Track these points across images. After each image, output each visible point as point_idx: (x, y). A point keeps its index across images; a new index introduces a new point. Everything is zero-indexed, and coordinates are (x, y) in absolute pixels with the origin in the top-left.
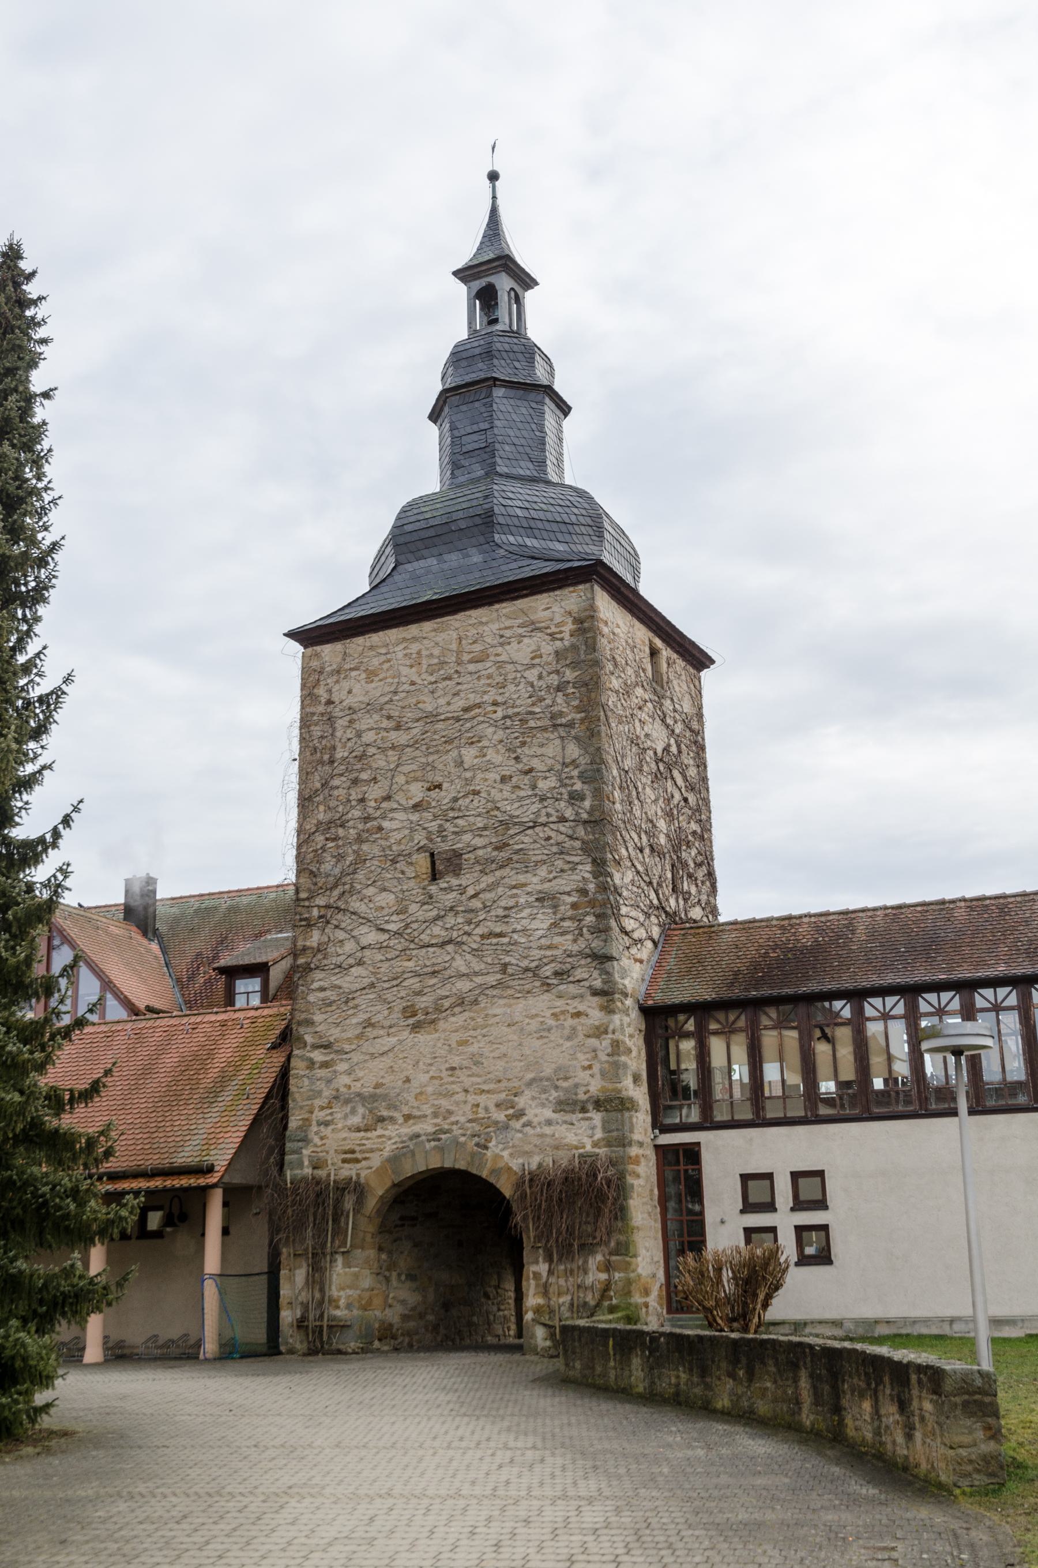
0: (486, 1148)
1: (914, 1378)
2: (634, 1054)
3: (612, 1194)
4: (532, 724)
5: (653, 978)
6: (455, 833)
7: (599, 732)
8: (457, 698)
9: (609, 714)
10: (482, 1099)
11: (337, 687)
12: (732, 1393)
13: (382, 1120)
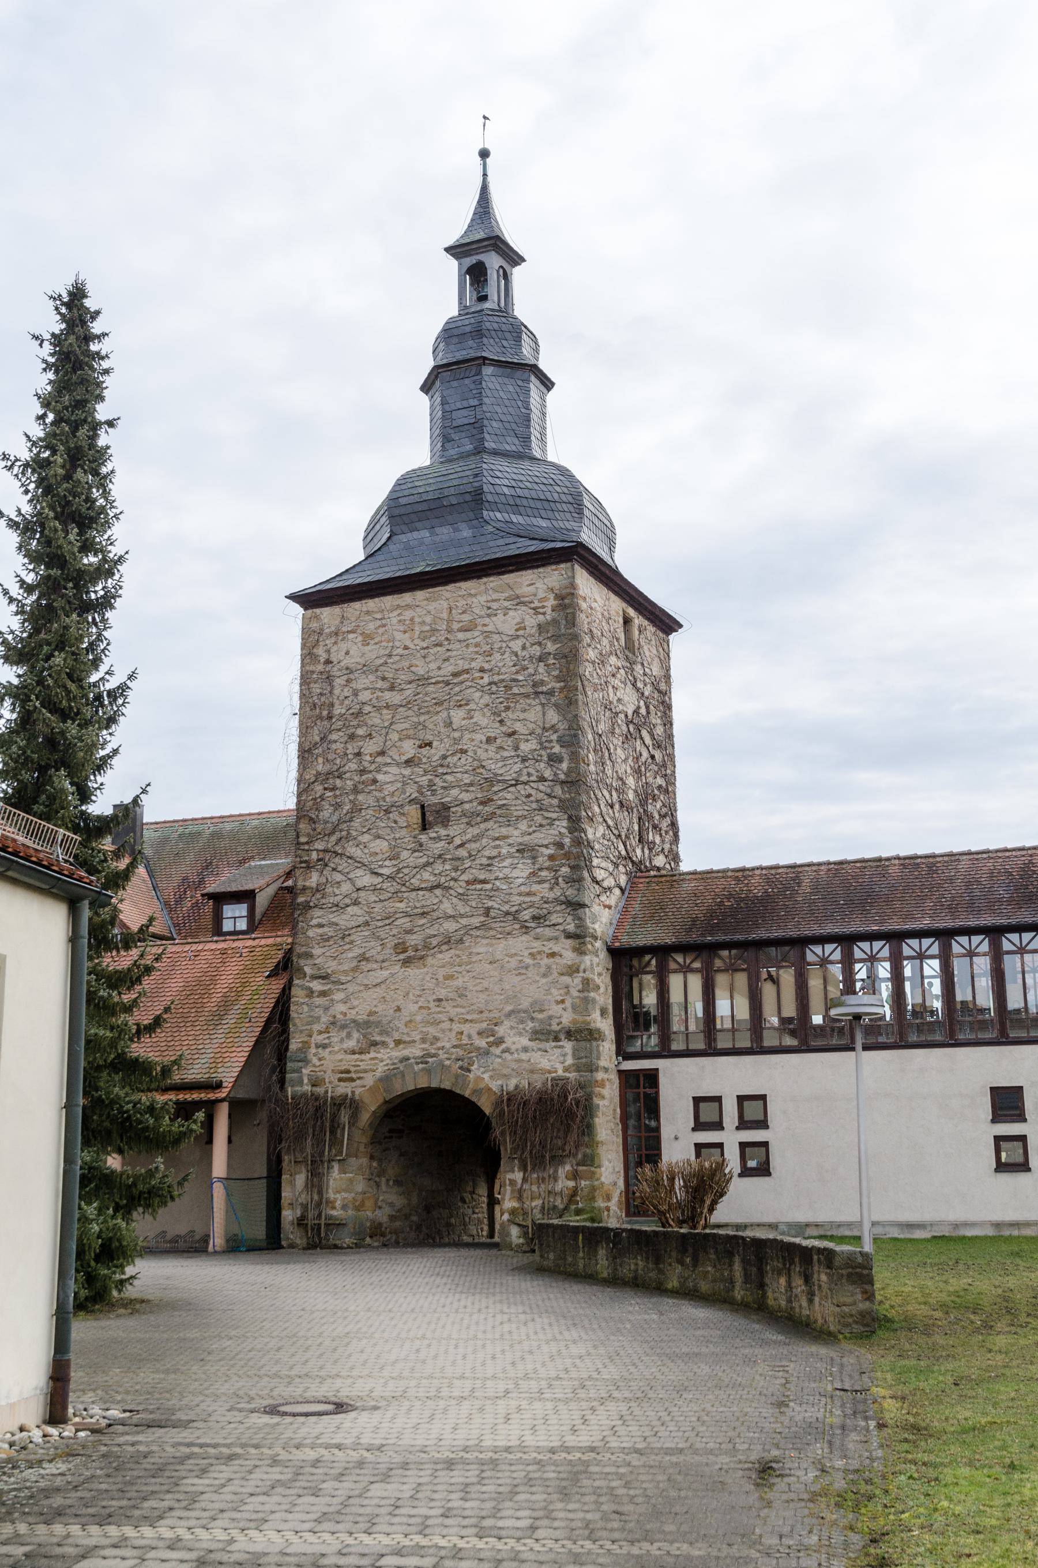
0: (469, 1071)
1: (815, 1257)
2: (602, 990)
3: (580, 1113)
4: (515, 690)
5: (620, 923)
6: (443, 788)
7: (576, 700)
8: (447, 663)
9: (586, 683)
10: (466, 1028)
11: (335, 648)
12: (680, 1276)
13: (375, 1044)
